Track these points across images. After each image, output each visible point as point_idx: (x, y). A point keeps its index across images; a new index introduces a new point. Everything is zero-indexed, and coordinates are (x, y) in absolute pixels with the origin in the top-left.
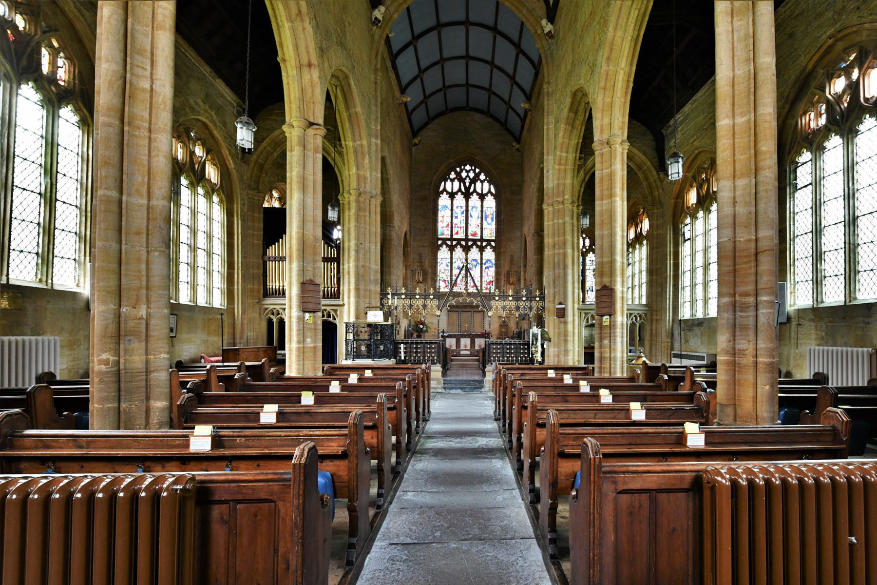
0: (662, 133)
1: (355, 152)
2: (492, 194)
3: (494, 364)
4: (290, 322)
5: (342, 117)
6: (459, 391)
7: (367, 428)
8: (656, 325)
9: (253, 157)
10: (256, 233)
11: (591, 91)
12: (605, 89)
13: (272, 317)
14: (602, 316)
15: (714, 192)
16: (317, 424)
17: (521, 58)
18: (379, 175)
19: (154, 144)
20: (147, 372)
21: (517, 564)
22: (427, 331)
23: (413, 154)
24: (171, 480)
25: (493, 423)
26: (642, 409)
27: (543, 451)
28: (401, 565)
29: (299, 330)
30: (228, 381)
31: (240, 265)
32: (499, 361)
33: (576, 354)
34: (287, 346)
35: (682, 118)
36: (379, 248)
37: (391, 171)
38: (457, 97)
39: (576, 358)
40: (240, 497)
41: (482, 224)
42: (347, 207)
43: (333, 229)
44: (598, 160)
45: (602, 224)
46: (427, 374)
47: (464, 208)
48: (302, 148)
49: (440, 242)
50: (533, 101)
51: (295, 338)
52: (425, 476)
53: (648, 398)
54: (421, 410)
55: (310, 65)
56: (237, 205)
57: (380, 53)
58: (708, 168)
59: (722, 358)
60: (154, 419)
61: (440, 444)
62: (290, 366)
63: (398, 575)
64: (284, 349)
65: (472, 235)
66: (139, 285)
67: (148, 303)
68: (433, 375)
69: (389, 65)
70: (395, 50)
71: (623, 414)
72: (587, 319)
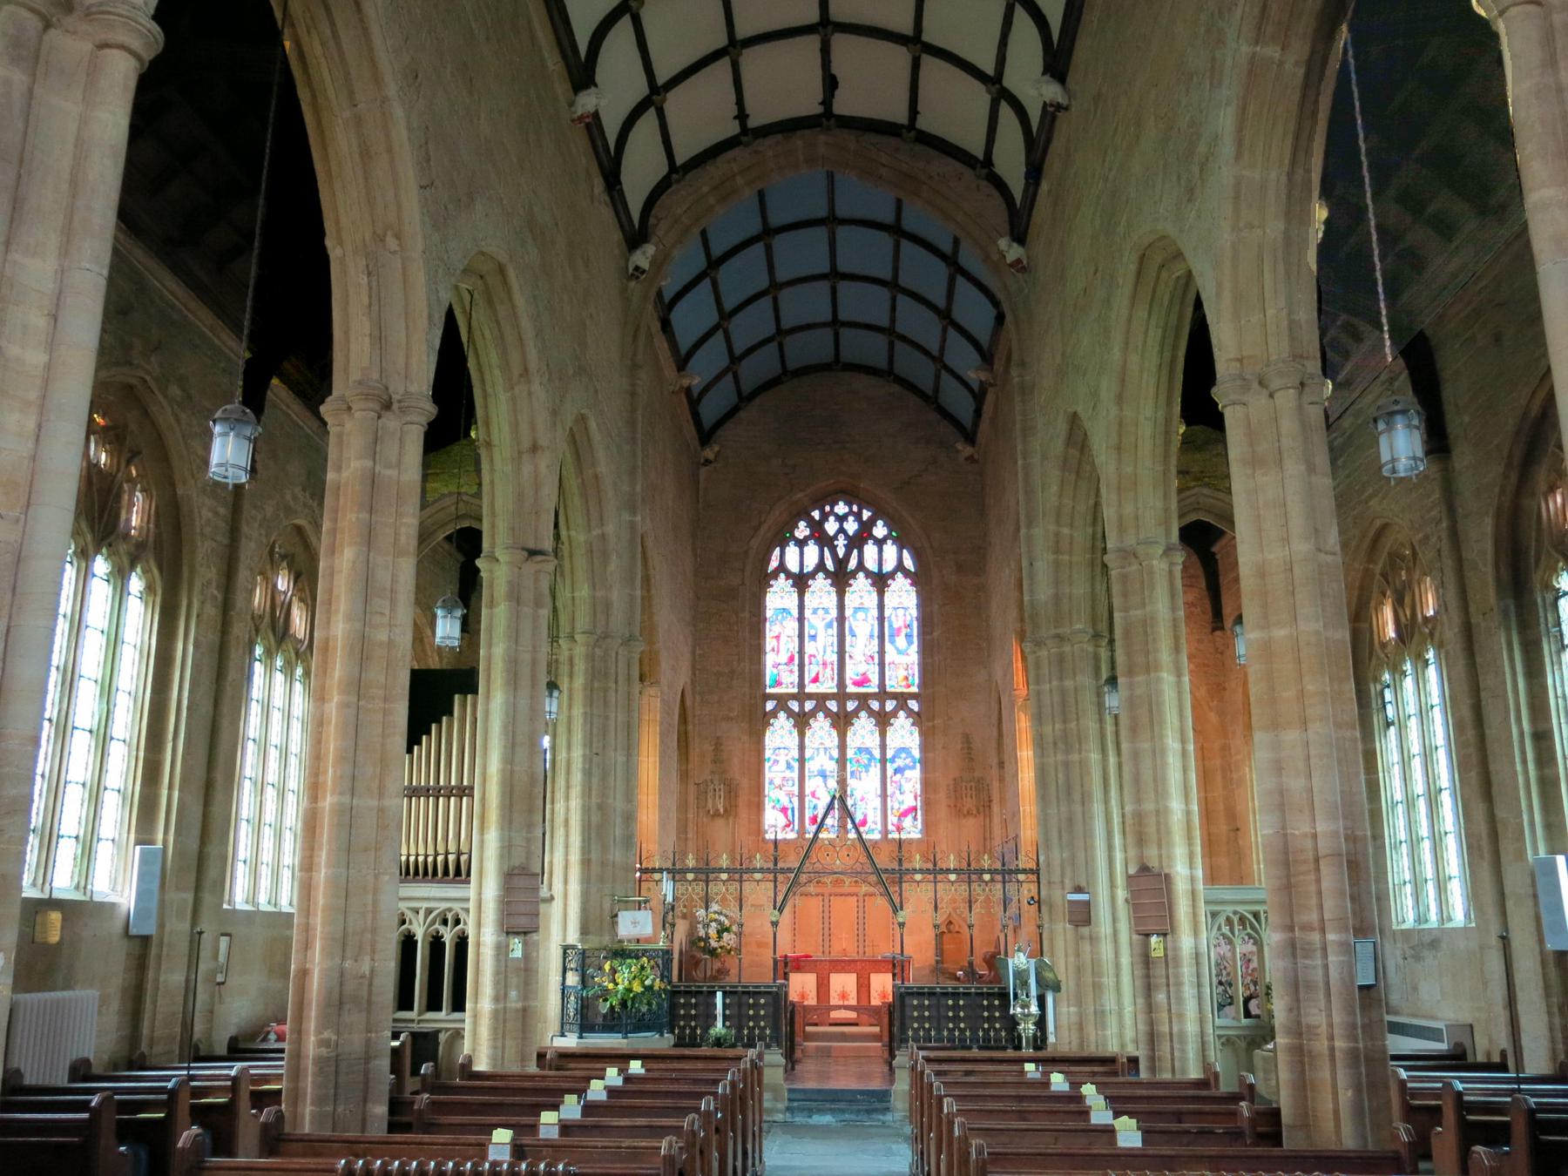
2: (907, 573)
23: (702, 486)
32: (916, 1040)
34: (468, 1005)
38: (810, 348)
39: (1129, 1034)
41: (882, 652)
46: (756, 1068)
47: (834, 613)
50: (998, 366)
55: (535, 448)
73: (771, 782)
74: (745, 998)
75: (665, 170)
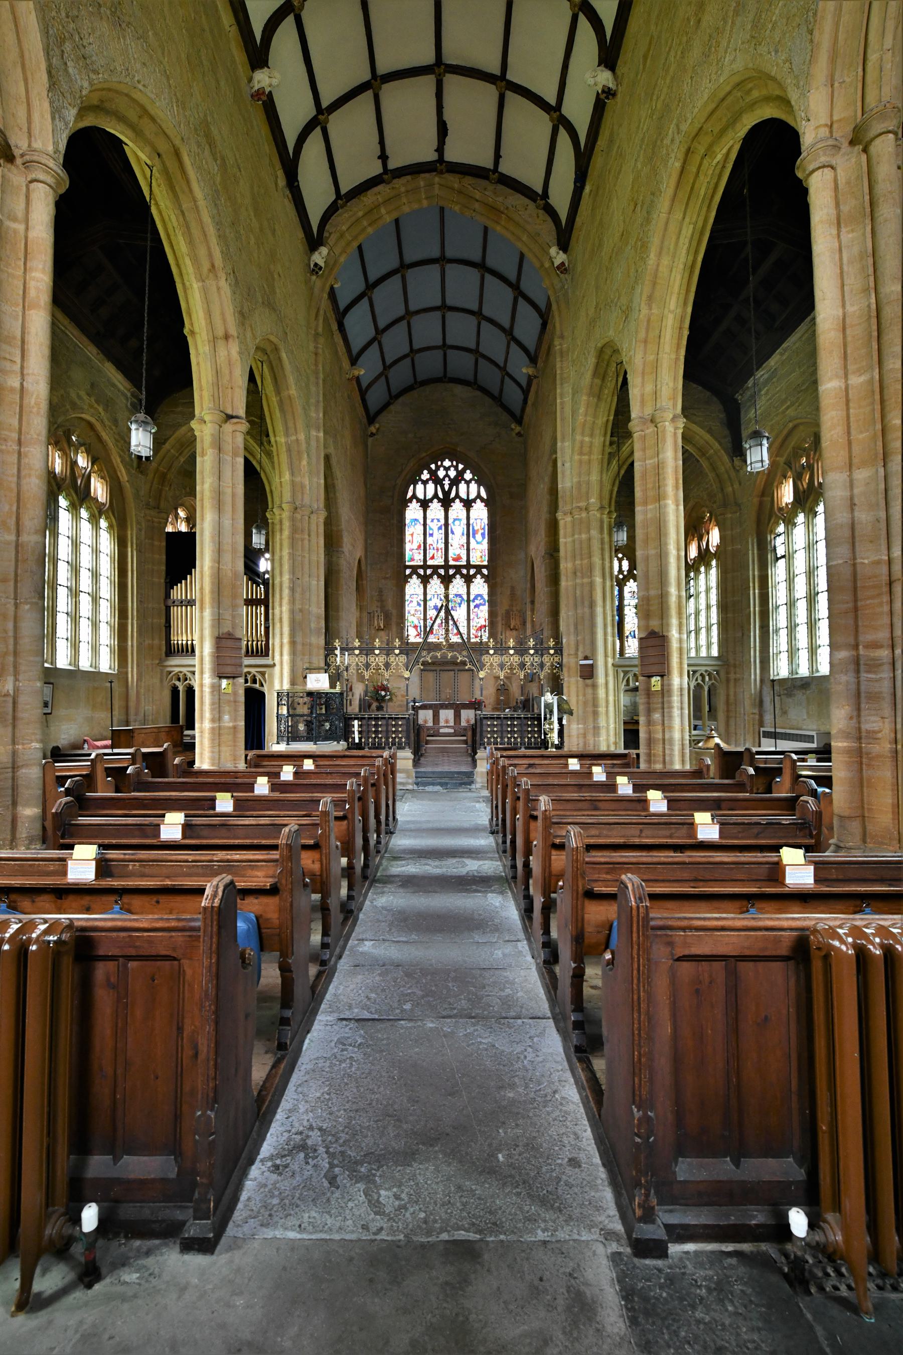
0: (736, 400)
1: (289, 450)
2: (482, 500)
3: (488, 748)
4: (202, 691)
5: (271, 404)
6: (438, 788)
7: (305, 847)
8: (735, 686)
9: (153, 464)
10: (155, 568)
11: (625, 346)
12: (645, 341)
13: (177, 683)
14: (650, 677)
15: (820, 484)
16: (237, 842)
17: (522, 303)
18: (322, 481)
19: (24, 461)
20: (14, 767)
21: (525, 1057)
22: (391, 700)
24: (43, 927)
25: (487, 838)
26: (713, 824)
27: (562, 888)
28: (355, 1053)
29: (212, 704)
30: (117, 774)
31: (135, 613)
33: (612, 733)
34: (197, 725)
35: (766, 376)
36: (322, 583)
37: (338, 473)
38: (429, 364)
39: (612, 739)
40: (133, 952)
42: (278, 527)
43: (260, 559)
44: (637, 446)
45: (646, 541)
46: (391, 767)
47: (442, 522)
48: (217, 451)
49: (408, 572)
50: (540, 364)
51: (207, 715)
52: (389, 918)
53: (723, 805)
54: (383, 817)
55: (227, 337)
56: (132, 530)
57: (322, 312)
58: (810, 449)
59: (840, 744)
60: (23, 832)
61: (411, 868)
62: (201, 754)
63: (350, 1068)
64: (193, 729)
65: (454, 560)
66: (5, 650)
67: (16, 674)
68: (400, 765)
69: (335, 327)
70: (342, 305)
71: (684, 830)
72: (628, 681)
73: (409, 612)
74: (390, 721)
75: (334, 197)
